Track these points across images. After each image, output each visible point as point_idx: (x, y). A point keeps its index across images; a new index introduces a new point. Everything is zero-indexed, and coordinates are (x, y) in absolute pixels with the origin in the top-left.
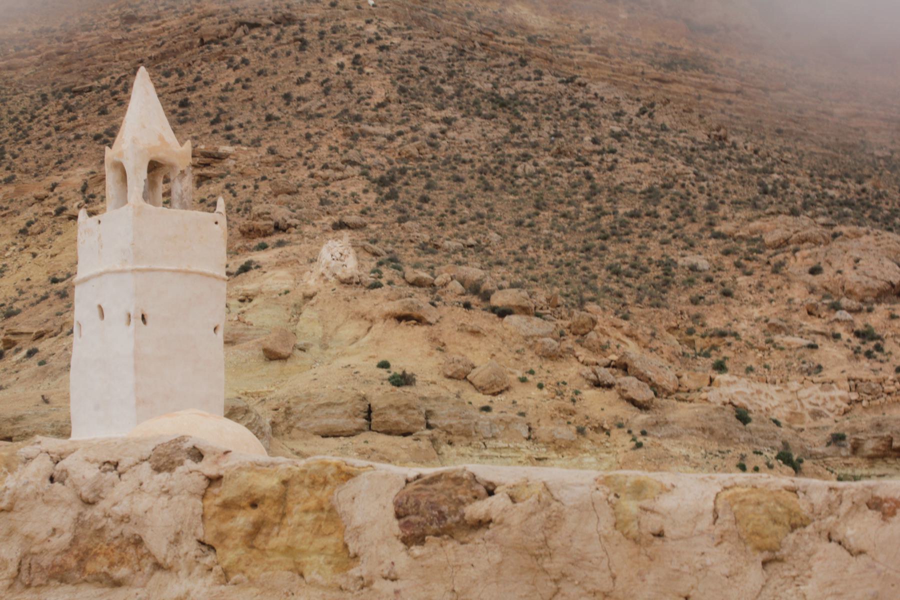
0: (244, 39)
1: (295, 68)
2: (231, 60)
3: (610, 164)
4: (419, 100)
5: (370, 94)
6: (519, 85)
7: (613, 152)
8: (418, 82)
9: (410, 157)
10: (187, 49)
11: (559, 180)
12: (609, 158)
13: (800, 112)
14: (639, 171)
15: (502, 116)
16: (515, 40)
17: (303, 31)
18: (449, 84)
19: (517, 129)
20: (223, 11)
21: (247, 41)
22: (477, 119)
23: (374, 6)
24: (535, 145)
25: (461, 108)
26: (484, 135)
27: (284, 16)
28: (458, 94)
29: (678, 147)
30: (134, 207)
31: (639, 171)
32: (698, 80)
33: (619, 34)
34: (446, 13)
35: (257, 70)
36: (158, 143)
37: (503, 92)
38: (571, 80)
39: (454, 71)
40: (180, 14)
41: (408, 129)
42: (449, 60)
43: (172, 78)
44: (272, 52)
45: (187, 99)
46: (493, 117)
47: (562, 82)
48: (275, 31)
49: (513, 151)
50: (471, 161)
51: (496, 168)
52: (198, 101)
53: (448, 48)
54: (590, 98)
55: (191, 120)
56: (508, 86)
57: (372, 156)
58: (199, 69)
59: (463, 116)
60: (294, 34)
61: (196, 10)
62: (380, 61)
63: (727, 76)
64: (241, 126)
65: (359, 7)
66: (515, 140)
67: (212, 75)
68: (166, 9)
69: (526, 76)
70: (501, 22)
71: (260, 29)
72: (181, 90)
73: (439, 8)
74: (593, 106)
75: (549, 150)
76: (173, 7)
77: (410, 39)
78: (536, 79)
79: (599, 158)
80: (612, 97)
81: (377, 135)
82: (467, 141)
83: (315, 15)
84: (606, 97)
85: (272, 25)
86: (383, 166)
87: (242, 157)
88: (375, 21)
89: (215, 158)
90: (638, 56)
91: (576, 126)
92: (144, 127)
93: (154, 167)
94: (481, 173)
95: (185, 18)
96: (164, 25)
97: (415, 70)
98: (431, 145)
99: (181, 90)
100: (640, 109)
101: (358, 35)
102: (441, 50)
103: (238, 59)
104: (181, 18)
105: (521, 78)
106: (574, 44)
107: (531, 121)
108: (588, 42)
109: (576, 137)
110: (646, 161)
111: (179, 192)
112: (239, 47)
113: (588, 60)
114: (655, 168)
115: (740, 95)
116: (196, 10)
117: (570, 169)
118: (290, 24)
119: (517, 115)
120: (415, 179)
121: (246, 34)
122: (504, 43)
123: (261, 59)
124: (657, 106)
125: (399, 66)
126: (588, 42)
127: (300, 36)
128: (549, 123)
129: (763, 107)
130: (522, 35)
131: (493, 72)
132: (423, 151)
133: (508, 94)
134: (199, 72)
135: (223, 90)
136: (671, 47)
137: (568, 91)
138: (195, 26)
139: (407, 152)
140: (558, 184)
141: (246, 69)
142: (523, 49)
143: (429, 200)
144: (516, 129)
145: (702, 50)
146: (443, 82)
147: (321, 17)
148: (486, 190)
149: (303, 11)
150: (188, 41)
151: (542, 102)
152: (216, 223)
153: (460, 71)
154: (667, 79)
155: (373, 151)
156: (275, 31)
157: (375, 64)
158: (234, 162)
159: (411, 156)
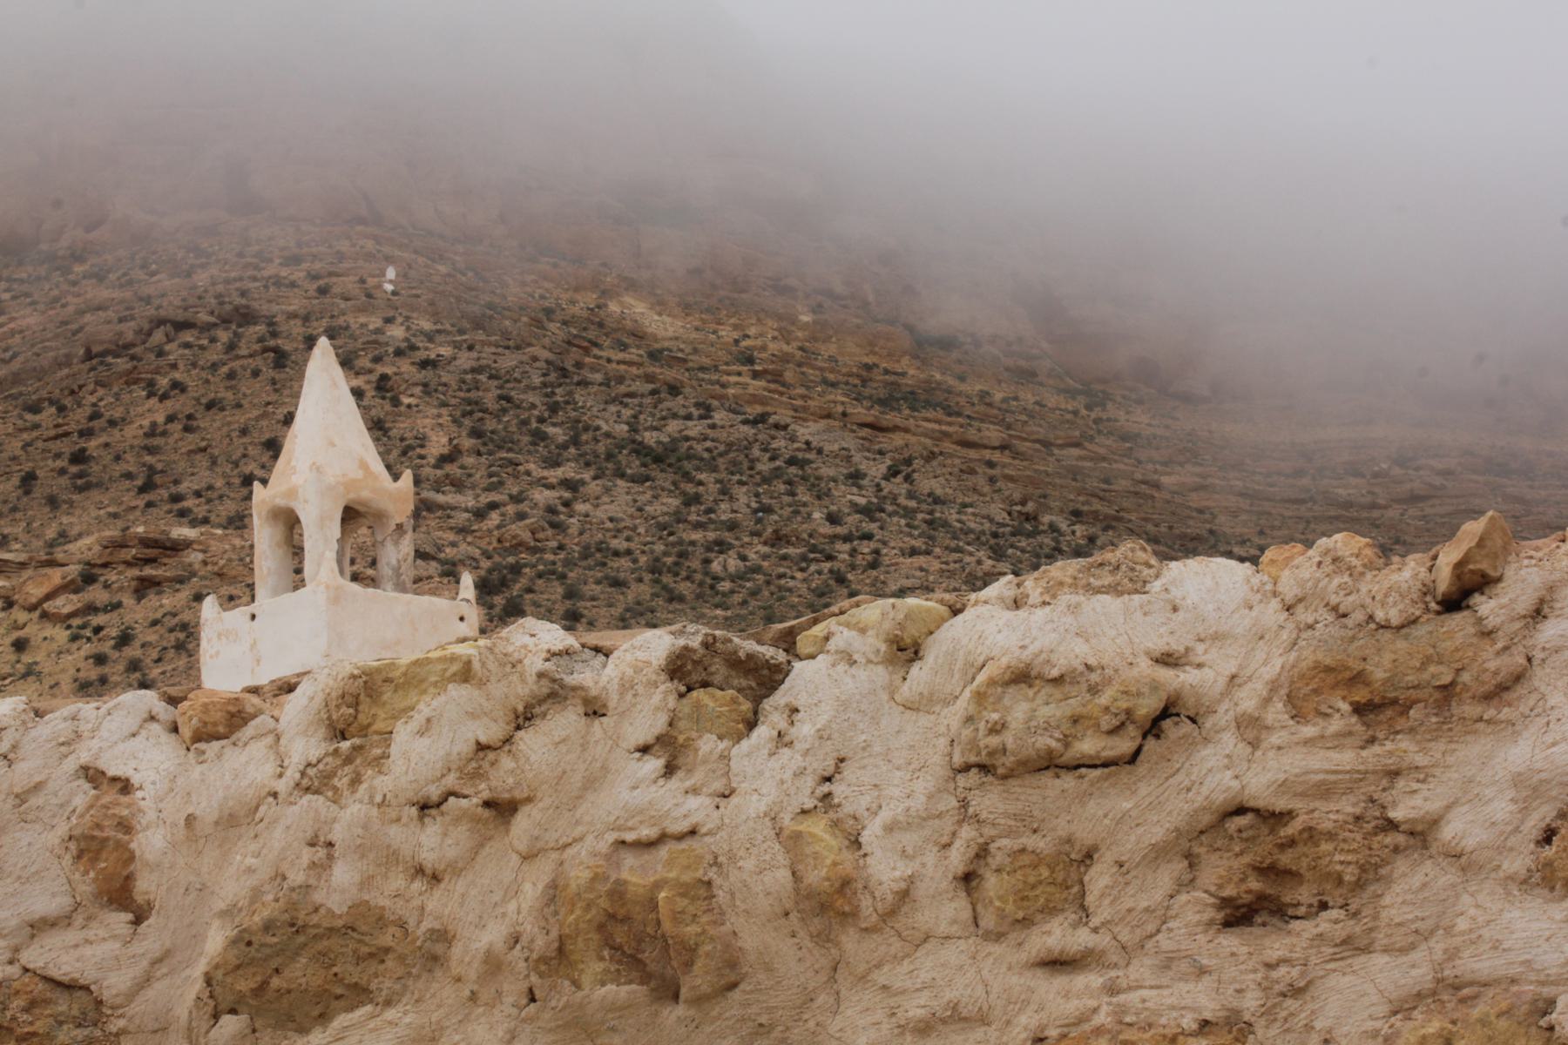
0: (167, 348)
1: (273, 397)
2: (151, 384)
3: (869, 558)
4: (510, 450)
5: (422, 440)
6: (673, 426)
7: (868, 537)
8: (500, 421)
9: (519, 546)
10: (60, 366)
11: (791, 583)
12: (866, 548)
13: (1107, 481)
14: (922, 569)
15: (664, 479)
16: (627, 357)
17: (274, 335)
18: (554, 425)
19: (697, 499)
20: (122, 302)
21: (174, 352)
22: (620, 482)
23: (394, 293)
24: (732, 526)
25: (588, 464)
26: (640, 510)
27: (237, 309)
28: (575, 441)
29: (971, 531)
30: (327, 587)
31: (922, 569)
32: (936, 427)
33: (801, 349)
34: (508, 309)
35: (204, 401)
36: (360, 474)
37: (650, 438)
38: (761, 419)
39: (557, 403)
40: (41, 307)
41: (506, 498)
42: (545, 385)
43: (45, 414)
44: (225, 369)
45: (83, 450)
46: (648, 479)
47: (745, 422)
48: (224, 336)
49: (697, 536)
50: (629, 552)
51: (676, 564)
52: (102, 452)
53: (537, 364)
54: (798, 450)
55: (99, 485)
56: (656, 429)
57: (453, 544)
58: (93, 399)
59: (595, 478)
60: (261, 340)
61: (70, 299)
62: (425, 385)
63: (982, 421)
64: (198, 494)
65: (369, 296)
66: (693, 518)
67: (121, 409)
68: (14, 298)
69: (682, 412)
70: (601, 325)
71: (195, 332)
72: (66, 434)
73: (497, 300)
74: (809, 462)
75: (757, 534)
76: (27, 295)
77: (470, 348)
78: (701, 417)
79: (847, 547)
80: (836, 447)
81: (453, 508)
82: (611, 520)
83: (292, 308)
84: (827, 448)
85: (215, 325)
86: (474, 559)
87: (215, 546)
88: (400, 320)
89: (166, 548)
90: (834, 385)
91: (793, 494)
92: (333, 445)
93: (350, 515)
94: (653, 572)
95: (51, 313)
96: (12, 325)
97: (489, 399)
98: (553, 525)
99: (66, 434)
100: (889, 468)
101: (376, 342)
102: (528, 368)
103: (163, 382)
104: (43, 313)
105: (675, 416)
106: (727, 364)
107: (714, 488)
108: (750, 360)
109: (797, 512)
110: (928, 553)
111: (394, 562)
112: (162, 362)
113: (751, 390)
114: (947, 563)
115: (1007, 452)
116: (70, 299)
117: (804, 565)
118: (248, 323)
119: (687, 476)
120: (540, 582)
121: (170, 340)
122: (609, 361)
123: (207, 381)
124: (917, 463)
125: (462, 394)
126: (750, 360)
127: (272, 343)
128: (744, 489)
129: (1048, 475)
130: (638, 347)
131: (626, 405)
132: (541, 535)
133: (659, 442)
134: (94, 405)
135: (146, 435)
136: (887, 372)
137: (760, 437)
138: (74, 326)
139: (514, 537)
140: (790, 590)
141: (182, 398)
142: (641, 371)
143: (582, 616)
144: (691, 500)
145: (938, 376)
146: (541, 420)
147: (302, 312)
148: (671, 600)
149: (270, 301)
150: (62, 352)
151: (721, 455)
152: (462, 619)
153: (567, 403)
154: (884, 424)
155: (451, 536)
156: (224, 336)
157: (418, 390)
158: (200, 556)
159: (520, 544)
